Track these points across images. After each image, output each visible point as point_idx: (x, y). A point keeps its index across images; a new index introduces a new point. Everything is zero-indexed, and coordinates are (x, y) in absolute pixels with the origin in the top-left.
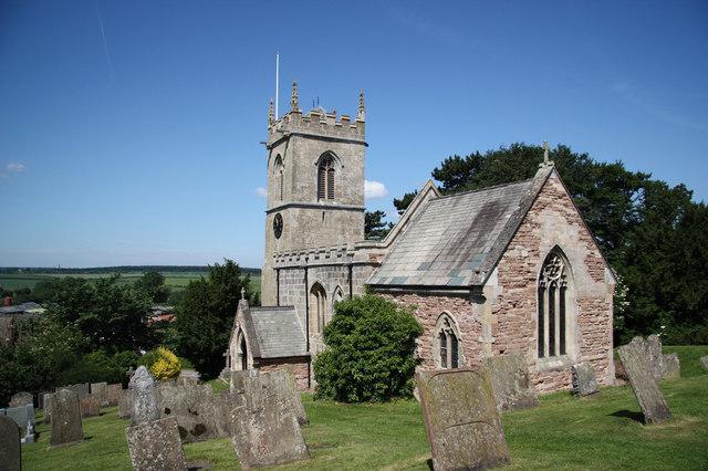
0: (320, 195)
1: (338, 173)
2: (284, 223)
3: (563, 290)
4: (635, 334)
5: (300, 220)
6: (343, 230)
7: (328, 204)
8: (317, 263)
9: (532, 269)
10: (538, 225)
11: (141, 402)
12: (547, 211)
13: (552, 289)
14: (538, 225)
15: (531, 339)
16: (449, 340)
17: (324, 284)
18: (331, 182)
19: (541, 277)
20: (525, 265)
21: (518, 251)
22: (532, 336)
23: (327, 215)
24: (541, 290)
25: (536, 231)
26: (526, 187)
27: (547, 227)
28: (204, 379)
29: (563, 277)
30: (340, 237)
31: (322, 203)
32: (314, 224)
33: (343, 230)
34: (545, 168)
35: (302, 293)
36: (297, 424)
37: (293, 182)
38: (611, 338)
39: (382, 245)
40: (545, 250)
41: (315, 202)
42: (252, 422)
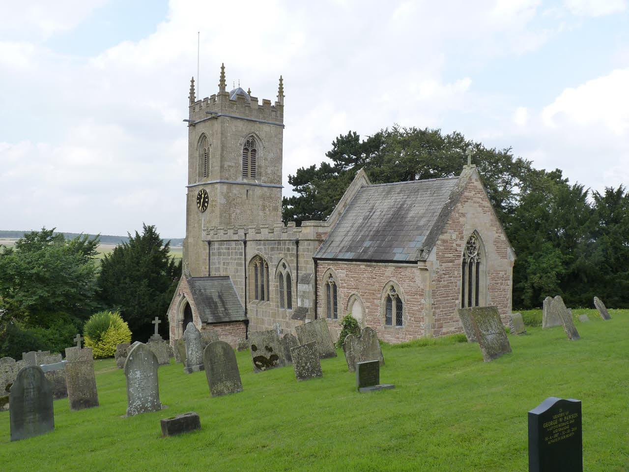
0: (245, 175)
1: (260, 153)
2: (211, 199)
3: (478, 264)
4: (546, 296)
5: (227, 197)
6: (264, 206)
7: (252, 182)
8: (258, 237)
9: (458, 249)
10: (463, 215)
11: (192, 350)
12: (470, 202)
13: (471, 264)
14: (463, 215)
15: (457, 302)
16: (394, 303)
17: (265, 257)
18: (253, 162)
19: (464, 255)
20: (454, 245)
21: (450, 235)
22: (457, 299)
23: (250, 192)
24: (464, 263)
25: (462, 219)
26: (450, 183)
27: (469, 216)
28: (134, 339)
29: (478, 254)
30: (261, 213)
31: (245, 181)
32: (239, 200)
33: (264, 206)
34: (469, 170)
35: (239, 264)
36: (379, 344)
37: (221, 161)
38: (74, 348)
39: (326, 225)
40: (467, 234)
41: (240, 180)
42: (356, 343)
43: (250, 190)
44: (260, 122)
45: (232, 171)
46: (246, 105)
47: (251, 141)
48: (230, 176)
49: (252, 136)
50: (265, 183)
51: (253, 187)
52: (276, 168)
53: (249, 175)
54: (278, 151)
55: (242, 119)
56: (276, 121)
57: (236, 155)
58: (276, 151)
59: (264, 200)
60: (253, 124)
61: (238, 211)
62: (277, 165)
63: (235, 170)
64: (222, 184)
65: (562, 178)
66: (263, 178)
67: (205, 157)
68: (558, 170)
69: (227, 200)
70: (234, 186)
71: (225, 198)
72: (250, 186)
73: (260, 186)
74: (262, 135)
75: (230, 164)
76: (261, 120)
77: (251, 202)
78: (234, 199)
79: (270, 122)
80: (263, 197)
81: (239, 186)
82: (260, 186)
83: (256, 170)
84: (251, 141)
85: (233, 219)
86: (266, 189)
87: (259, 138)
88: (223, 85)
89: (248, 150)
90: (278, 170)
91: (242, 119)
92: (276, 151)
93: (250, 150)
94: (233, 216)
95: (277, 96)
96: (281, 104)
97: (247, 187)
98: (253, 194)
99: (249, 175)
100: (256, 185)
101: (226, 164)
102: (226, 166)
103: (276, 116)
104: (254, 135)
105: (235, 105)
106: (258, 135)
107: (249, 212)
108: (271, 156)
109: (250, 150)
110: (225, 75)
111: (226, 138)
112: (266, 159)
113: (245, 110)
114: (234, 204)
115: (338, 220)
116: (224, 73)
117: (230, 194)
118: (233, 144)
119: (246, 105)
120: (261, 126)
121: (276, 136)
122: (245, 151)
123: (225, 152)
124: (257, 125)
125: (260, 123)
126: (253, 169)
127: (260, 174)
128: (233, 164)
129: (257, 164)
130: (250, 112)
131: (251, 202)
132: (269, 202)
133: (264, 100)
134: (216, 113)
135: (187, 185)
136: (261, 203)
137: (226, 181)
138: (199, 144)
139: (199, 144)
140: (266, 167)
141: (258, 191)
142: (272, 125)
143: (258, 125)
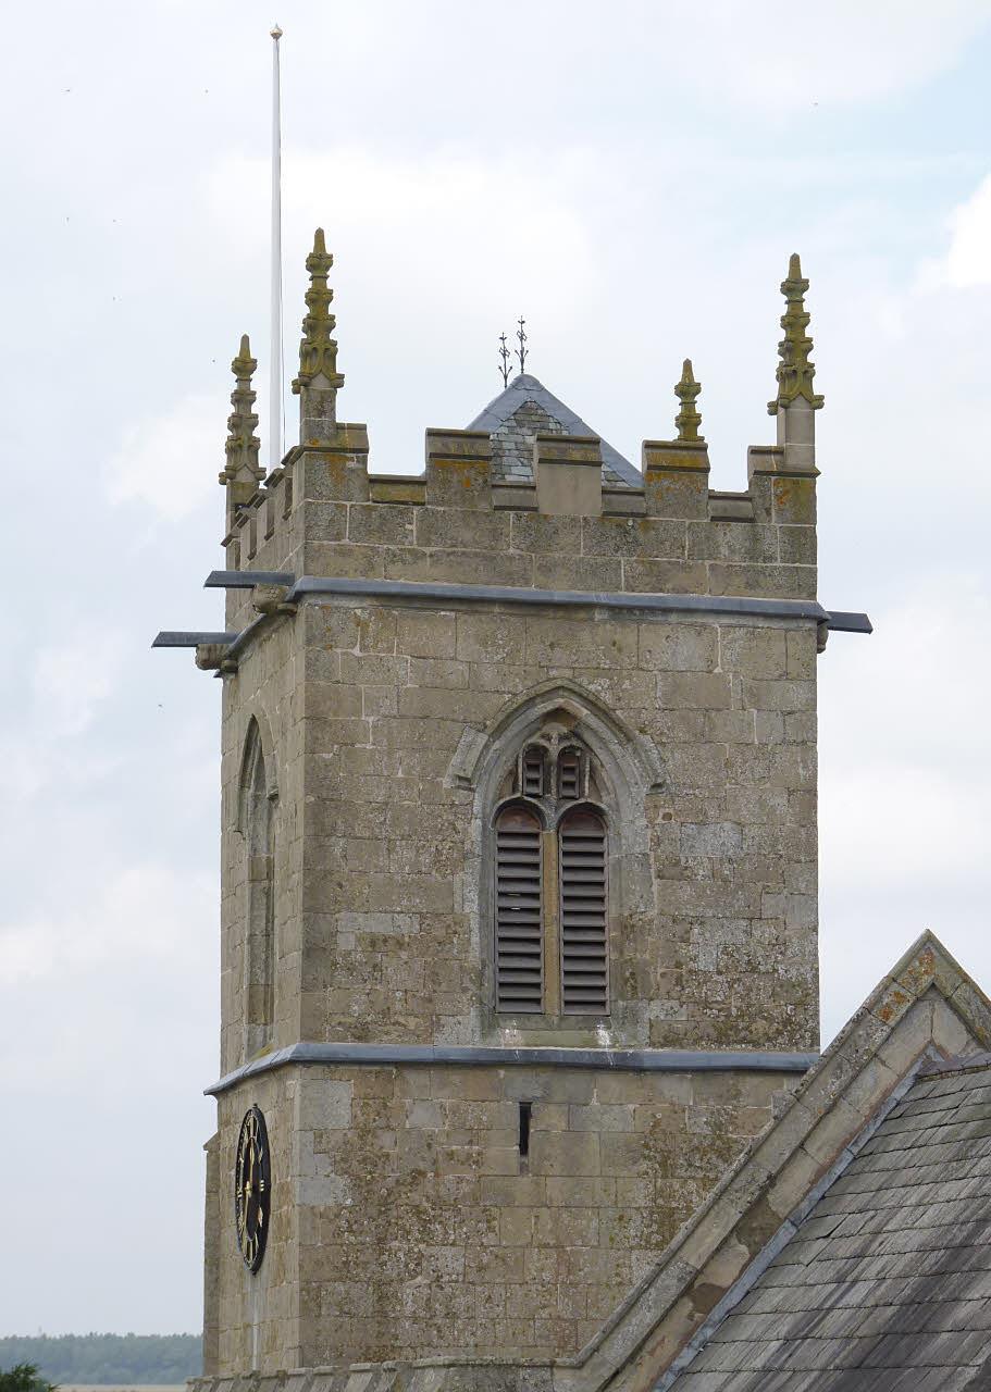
7: (564, 1043)
18: (586, 897)
23: (549, 1120)
31: (511, 1038)
41: (461, 1034)
43: (546, 1099)
44: (618, 611)
45: (400, 973)
46: (499, 498)
47: (554, 749)
48: (386, 1012)
49: (558, 714)
51: (572, 1083)
53: (552, 996)
54: (779, 801)
55: (470, 603)
56: (751, 586)
57: (425, 859)
58: (761, 803)
59: (666, 1166)
61: (450, 1260)
62: (770, 905)
63: (418, 965)
64: (317, 1070)
66: (654, 1011)
69: (357, 1184)
70: (414, 1078)
71: (342, 1165)
72: (545, 1076)
73: (626, 1066)
74: (640, 697)
75: (379, 925)
76: (624, 596)
77: (555, 1189)
78: (422, 1174)
79: (705, 598)
81: (455, 1077)
82: (626, 1066)
83: (610, 953)
84: (554, 749)
85: (415, 1319)
86: (678, 1090)
87: (617, 726)
88: (320, 384)
89: (535, 814)
90: (780, 944)
91: (470, 603)
92: (761, 803)
93: (552, 816)
94: (411, 1294)
96: (793, 462)
97: (525, 1085)
98: (575, 1133)
99: (552, 996)
100: (597, 1066)
101: (350, 928)
102: (346, 942)
103: (752, 554)
105: (416, 510)
106: (607, 698)
107: (540, 1265)
108: (715, 842)
109: (552, 816)
110: (809, 332)
111: (348, 744)
112: (673, 871)
113: (496, 535)
114: (418, 1211)
115: (686, 1340)
117: (386, 1140)
118: (407, 783)
119: (499, 498)
120: (627, 635)
121: (755, 697)
122: (515, 825)
123: (338, 846)
124: (594, 638)
126: (585, 950)
127: (635, 983)
128: (407, 926)
129: (612, 909)
130: (532, 547)
131: (555, 1189)
133: (432, 434)
134: (288, 580)
135: (215, 1079)
136: (640, 1195)
137: (350, 1047)
138: (250, 792)
139: (250, 792)
140: (682, 926)
142: (716, 623)
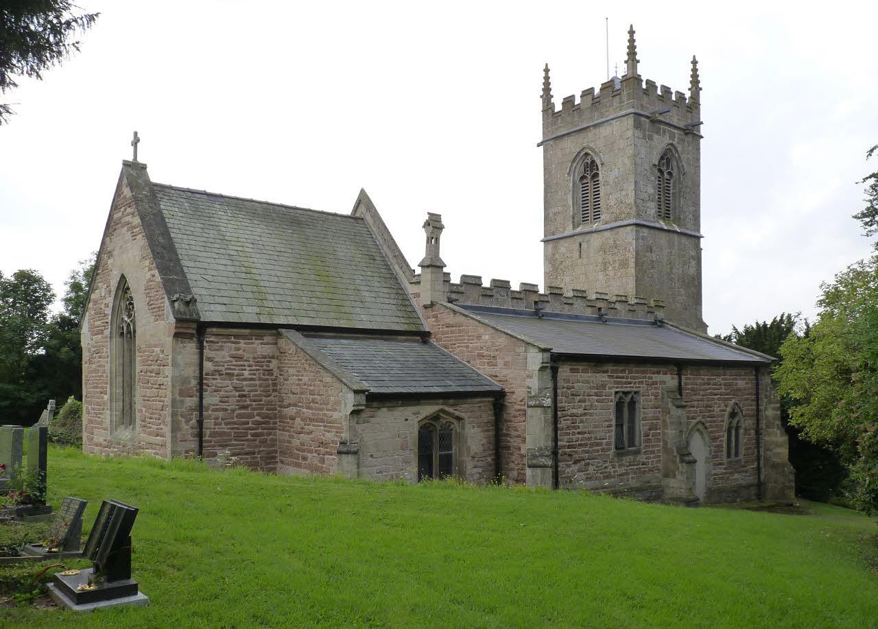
23: (584, 245)
30: (601, 276)
32: (568, 262)
44: (595, 126)
50: (606, 223)
51: (587, 237)
52: (623, 193)
60: (582, 135)
65: (513, 288)
67: (131, 362)
68: (146, 165)
75: (556, 210)
80: (603, 249)
81: (568, 240)
86: (607, 234)
95: (626, 62)
97: (579, 239)
104: (590, 152)
109: (589, 177)
110: (550, 81)
114: (562, 269)
116: (634, 41)
125: (595, 126)
132: (613, 254)
141: (596, 241)
143: (593, 131)
